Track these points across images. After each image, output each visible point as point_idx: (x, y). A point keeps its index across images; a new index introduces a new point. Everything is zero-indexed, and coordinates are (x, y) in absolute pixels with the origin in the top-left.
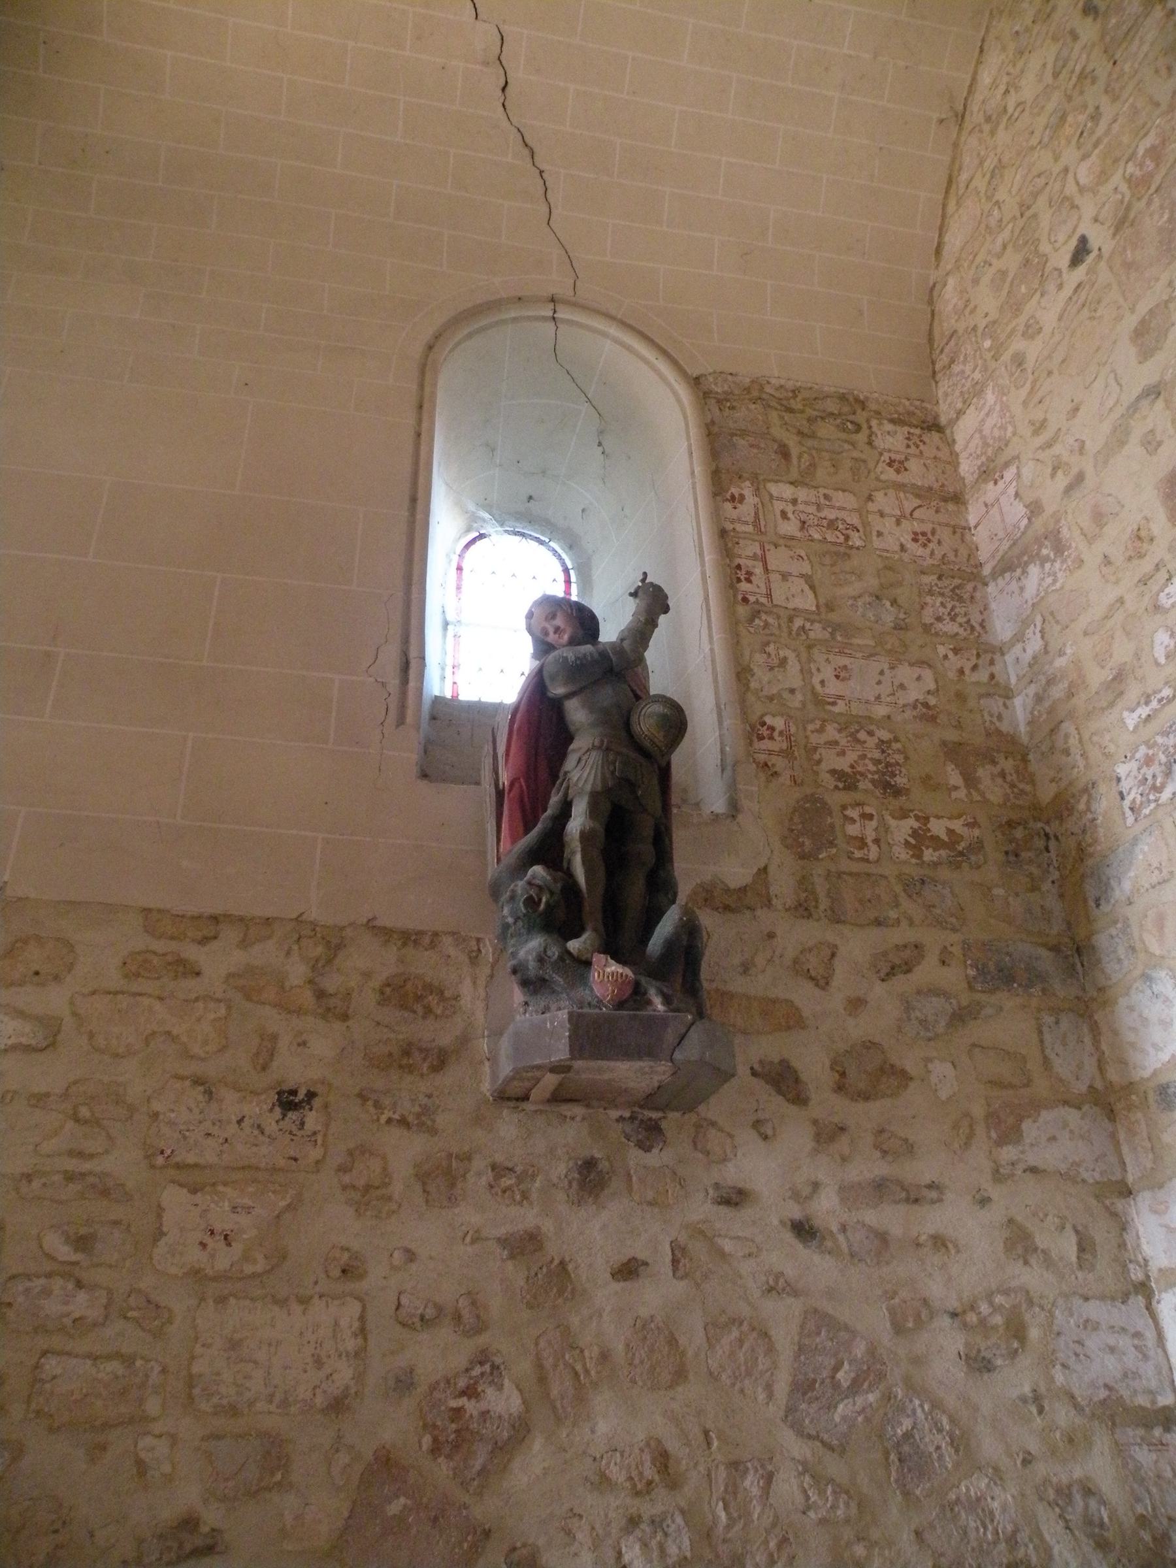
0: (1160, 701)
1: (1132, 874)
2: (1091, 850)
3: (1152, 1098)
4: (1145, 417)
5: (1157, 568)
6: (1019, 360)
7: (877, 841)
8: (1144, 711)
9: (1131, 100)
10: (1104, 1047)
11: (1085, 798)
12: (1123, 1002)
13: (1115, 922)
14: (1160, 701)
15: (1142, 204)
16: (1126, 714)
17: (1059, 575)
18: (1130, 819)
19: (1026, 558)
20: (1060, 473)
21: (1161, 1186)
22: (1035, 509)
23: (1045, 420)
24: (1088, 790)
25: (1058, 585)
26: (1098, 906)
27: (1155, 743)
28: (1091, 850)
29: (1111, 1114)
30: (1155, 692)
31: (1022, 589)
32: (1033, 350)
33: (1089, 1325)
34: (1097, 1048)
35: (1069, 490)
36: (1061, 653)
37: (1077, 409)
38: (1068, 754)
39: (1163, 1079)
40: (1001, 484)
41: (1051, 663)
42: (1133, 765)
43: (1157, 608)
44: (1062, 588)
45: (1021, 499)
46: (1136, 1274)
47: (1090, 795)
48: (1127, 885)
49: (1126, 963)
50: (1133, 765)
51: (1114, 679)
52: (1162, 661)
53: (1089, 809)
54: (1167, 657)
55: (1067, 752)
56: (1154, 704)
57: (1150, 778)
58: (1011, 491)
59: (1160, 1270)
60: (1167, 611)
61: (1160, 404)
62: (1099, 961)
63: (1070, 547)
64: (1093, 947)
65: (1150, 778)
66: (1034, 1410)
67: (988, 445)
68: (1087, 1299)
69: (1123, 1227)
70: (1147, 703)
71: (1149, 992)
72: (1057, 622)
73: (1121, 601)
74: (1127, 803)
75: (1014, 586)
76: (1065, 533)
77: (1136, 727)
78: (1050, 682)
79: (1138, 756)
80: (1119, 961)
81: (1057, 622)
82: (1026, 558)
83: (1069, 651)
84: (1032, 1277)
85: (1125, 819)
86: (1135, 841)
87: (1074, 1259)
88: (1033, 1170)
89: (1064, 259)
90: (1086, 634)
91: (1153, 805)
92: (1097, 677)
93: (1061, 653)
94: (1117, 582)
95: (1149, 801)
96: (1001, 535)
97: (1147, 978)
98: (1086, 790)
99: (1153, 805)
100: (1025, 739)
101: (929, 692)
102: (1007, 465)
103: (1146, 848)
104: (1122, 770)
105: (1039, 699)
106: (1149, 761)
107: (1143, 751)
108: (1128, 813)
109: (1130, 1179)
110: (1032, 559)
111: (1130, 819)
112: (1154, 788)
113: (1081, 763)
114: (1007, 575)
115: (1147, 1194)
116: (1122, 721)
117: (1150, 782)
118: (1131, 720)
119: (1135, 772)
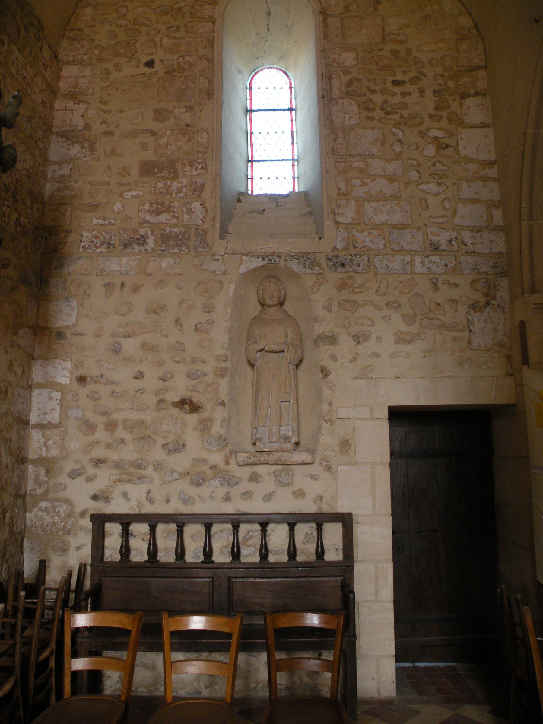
0: (109, 222)
1: (75, 266)
2: (60, 250)
3: (54, 334)
4: (146, 137)
5: (128, 184)
6: (107, 72)
7: (8, 216)
8: (102, 222)
9: (191, 39)
10: (40, 312)
11: (65, 234)
12: (54, 302)
13: (62, 277)
14: (109, 222)
15: (179, 75)
16: (94, 218)
17: (88, 157)
18: (81, 250)
19: (75, 140)
20: (104, 125)
21: (47, 360)
22: (87, 127)
23: (107, 102)
24: (68, 232)
25: (85, 160)
26: (56, 269)
27: (101, 233)
28: (60, 250)
29: (36, 334)
30: (108, 219)
31: (69, 149)
32: (115, 75)
33: (20, 395)
34: (38, 313)
35: (105, 133)
36: (76, 182)
37: (122, 111)
38: (64, 216)
39: (61, 330)
40: (76, 106)
41: (70, 182)
42: (90, 235)
43: (121, 195)
44: (87, 162)
45: (83, 118)
46: (30, 383)
47: (68, 234)
48: (71, 268)
49: (60, 291)
50: (90, 235)
51: (95, 205)
52: (116, 212)
53: (65, 237)
54: (118, 212)
55: (64, 215)
56: (107, 222)
57: (95, 242)
58: (81, 112)
59: (37, 383)
60: (124, 198)
61: (153, 138)
62: (49, 286)
63: (97, 152)
64: (48, 281)
65: (95, 242)
66: (4, 417)
67: (78, 87)
68: (21, 387)
69: (30, 368)
70: (104, 220)
71: (66, 304)
72: (79, 171)
73: (109, 183)
74: (82, 245)
75: (65, 145)
76: (97, 145)
77: (96, 224)
78: (66, 188)
79: (93, 233)
80: (58, 289)
81: (79, 171)
82: (75, 140)
83: (79, 184)
84: (11, 378)
85: (79, 249)
86: (80, 258)
87: (20, 375)
88: (18, 345)
89: (143, 61)
90: (90, 183)
91: (92, 251)
92: (87, 199)
93: (76, 182)
94: (110, 176)
95: (91, 249)
96: (68, 123)
97: (67, 299)
98: (67, 231)
99: (92, 251)
100: (46, 199)
101: (31, 167)
102: (83, 102)
103: (84, 262)
104: (85, 234)
105: (59, 190)
106: (96, 237)
107: (95, 233)
108: (81, 248)
109: (35, 354)
110: (78, 142)
111: (81, 250)
112: (95, 246)
113: (68, 221)
114: (64, 139)
115: (41, 361)
116: (92, 220)
117: (94, 243)
118: (95, 221)
119: (90, 237)
